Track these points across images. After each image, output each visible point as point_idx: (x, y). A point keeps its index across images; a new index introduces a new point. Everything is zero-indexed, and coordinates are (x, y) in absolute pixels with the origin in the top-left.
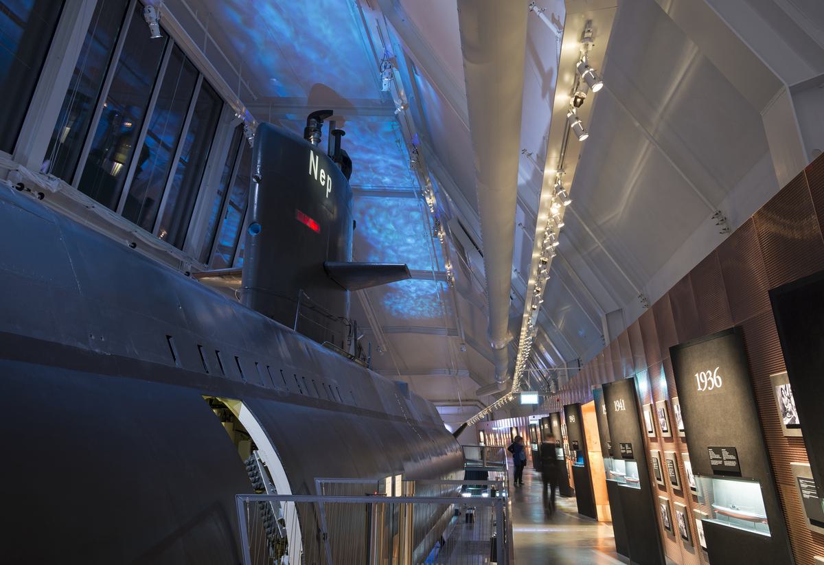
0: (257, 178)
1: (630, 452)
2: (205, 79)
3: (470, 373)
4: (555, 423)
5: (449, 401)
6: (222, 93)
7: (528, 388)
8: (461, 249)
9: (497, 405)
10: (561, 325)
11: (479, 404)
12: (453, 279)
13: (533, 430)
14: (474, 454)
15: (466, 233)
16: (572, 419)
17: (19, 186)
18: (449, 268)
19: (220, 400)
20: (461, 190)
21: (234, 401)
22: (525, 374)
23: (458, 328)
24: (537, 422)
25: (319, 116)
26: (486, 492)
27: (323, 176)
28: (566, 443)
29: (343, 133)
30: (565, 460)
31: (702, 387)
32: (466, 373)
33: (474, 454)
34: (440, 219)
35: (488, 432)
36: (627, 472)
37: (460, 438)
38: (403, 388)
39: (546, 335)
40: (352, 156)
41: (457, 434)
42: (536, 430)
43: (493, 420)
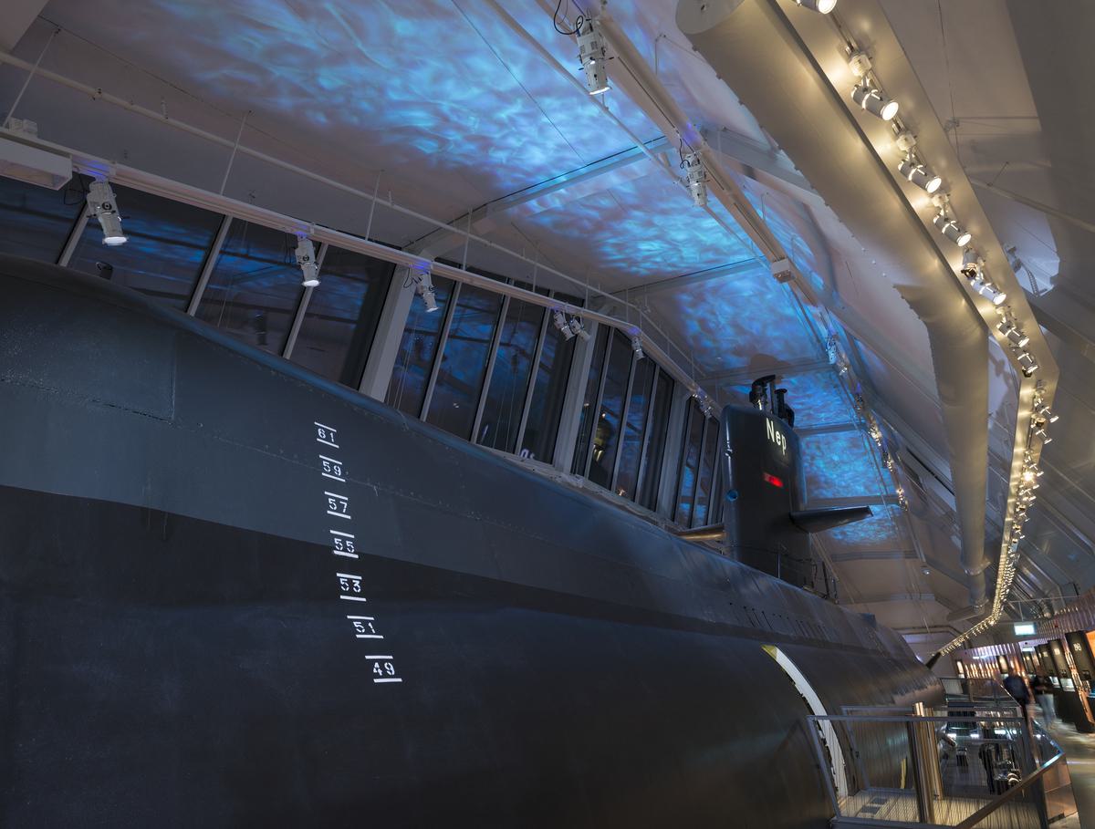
0: (729, 453)
2: (661, 368)
4: (1057, 651)
5: (914, 628)
6: (675, 375)
7: (1020, 618)
8: (916, 477)
10: (1045, 548)
11: (952, 631)
12: (906, 503)
13: (1028, 658)
14: (954, 688)
16: (1077, 647)
18: (900, 493)
21: (771, 647)
22: (1009, 596)
23: (916, 548)
24: (1031, 649)
25: (761, 382)
26: (976, 732)
27: (778, 437)
28: (1074, 672)
29: (785, 391)
30: (1077, 693)
33: (954, 688)
34: (890, 448)
35: (968, 661)
37: (935, 667)
38: (870, 620)
39: (1029, 560)
40: (793, 406)
41: (931, 663)
42: (1031, 658)
43: (971, 648)
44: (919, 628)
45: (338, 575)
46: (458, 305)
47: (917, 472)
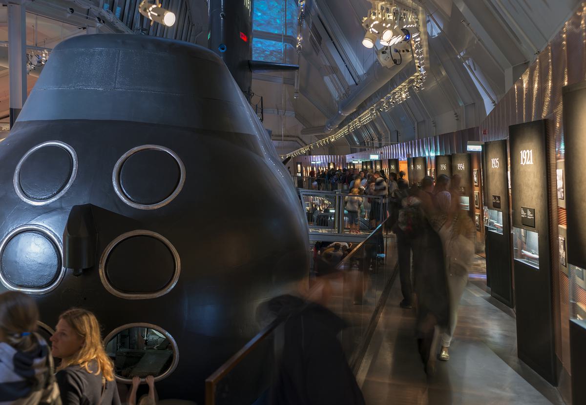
1: (499, 202)
3: (296, 115)
9: (319, 144)
15: (329, 35)
20: (328, 5)
31: (523, 162)
32: (291, 114)
45: (538, 268)
46: (311, 136)
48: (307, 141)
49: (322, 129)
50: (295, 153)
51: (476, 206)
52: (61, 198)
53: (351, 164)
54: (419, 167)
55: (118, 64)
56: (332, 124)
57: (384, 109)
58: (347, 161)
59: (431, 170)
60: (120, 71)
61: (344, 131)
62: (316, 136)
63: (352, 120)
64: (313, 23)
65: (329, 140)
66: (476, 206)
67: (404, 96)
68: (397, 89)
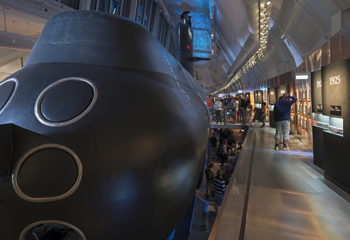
8: (219, 49)
15: (221, 44)
17: (46, 10)
19: (33, 48)
31: (318, 86)
36: (259, 106)
44: (207, 88)
47: (220, 48)
48: (217, 89)
49: (222, 84)
50: (212, 94)
51: (292, 111)
52: (5, 110)
53: (232, 96)
54: (259, 94)
55: (68, 27)
56: (225, 82)
57: (244, 72)
58: (231, 95)
59: (265, 95)
60: (68, 31)
61: (229, 84)
62: (295, 148)
63: (232, 79)
64: (217, 43)
65: (224, 88)
66: (292, 111)
67: (253, 63)
68: (250, 61)
